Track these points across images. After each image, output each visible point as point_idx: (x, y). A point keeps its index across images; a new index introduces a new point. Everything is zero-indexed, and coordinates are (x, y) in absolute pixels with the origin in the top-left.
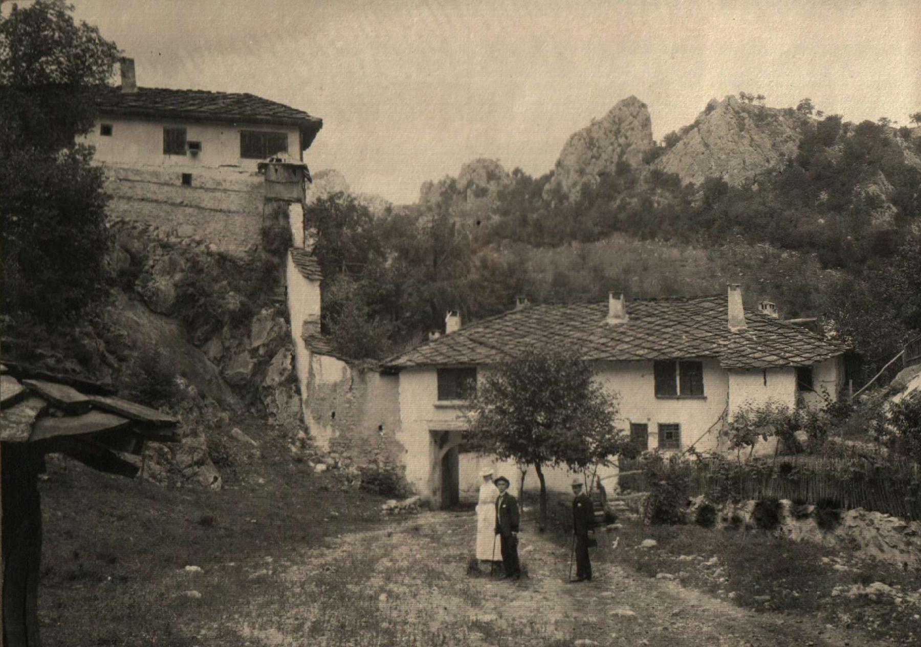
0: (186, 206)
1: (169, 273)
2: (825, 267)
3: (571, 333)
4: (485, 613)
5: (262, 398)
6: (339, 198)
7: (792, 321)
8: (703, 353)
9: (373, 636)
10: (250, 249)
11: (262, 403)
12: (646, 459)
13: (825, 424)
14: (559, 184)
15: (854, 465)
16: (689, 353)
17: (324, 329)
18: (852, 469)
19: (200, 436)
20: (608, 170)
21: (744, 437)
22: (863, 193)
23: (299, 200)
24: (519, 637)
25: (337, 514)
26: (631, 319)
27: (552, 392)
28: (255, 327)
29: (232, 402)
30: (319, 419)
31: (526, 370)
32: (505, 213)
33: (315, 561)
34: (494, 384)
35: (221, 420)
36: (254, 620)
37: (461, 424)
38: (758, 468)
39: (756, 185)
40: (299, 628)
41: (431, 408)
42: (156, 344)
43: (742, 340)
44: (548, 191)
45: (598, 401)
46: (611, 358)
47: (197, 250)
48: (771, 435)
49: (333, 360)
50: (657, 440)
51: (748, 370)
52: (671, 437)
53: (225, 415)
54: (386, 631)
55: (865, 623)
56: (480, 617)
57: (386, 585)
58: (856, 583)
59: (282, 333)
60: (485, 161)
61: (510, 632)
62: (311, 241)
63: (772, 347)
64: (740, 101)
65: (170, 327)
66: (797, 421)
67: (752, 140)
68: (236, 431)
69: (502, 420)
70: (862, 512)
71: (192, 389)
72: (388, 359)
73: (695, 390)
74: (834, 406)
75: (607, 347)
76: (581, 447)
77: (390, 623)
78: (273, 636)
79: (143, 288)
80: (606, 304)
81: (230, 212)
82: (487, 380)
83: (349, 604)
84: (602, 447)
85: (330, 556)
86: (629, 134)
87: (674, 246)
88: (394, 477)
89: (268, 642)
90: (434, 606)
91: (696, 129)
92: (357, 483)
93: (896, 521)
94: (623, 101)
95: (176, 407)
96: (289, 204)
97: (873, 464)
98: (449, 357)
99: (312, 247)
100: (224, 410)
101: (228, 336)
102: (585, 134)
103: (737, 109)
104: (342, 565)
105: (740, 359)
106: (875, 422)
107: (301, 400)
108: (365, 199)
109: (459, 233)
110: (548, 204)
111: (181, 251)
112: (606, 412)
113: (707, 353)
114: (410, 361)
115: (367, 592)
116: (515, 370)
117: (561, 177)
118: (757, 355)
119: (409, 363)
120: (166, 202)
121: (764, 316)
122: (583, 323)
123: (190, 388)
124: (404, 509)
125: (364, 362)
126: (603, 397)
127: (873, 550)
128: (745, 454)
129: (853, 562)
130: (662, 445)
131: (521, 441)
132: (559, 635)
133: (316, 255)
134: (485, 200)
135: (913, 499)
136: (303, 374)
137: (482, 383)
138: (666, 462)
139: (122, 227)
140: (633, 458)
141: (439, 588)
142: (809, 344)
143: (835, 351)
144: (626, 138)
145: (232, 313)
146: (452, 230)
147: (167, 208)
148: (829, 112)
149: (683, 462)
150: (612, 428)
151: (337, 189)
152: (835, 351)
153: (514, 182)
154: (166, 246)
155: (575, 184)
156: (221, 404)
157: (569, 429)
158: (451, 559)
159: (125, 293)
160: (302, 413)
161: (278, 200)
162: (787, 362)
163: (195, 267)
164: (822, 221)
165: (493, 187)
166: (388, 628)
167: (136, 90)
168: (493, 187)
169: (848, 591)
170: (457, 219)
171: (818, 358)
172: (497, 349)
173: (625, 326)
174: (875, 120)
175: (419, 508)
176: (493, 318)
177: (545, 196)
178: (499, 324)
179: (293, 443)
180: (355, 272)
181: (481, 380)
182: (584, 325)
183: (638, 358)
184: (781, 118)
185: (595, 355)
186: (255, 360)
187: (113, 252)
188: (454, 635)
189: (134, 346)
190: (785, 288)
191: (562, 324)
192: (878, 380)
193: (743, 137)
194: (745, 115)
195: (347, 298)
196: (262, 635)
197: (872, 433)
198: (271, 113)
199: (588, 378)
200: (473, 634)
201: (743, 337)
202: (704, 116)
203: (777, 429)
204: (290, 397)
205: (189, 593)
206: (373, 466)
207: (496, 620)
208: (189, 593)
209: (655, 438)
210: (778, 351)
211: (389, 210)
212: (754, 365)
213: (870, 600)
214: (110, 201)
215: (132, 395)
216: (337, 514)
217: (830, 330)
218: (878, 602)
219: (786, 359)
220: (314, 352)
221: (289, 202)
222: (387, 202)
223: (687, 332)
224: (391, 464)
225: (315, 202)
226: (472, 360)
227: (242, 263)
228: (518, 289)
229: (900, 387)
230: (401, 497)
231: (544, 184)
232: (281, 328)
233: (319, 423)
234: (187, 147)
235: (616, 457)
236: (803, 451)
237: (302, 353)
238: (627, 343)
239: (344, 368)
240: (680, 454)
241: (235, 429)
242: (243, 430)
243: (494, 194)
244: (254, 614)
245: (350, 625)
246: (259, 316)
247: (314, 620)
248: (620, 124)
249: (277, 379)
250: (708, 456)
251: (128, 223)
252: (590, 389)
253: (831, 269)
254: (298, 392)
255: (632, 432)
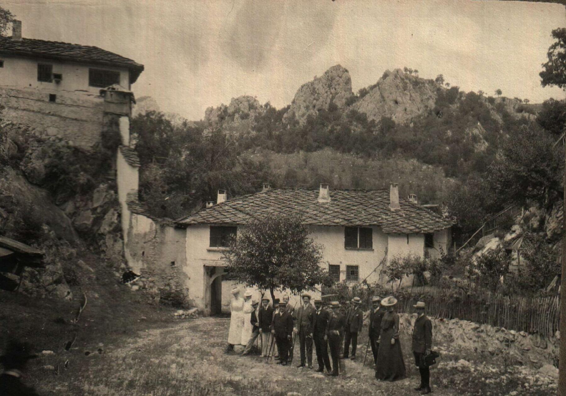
0: (53, 115)
1: (41, 159)
2: (447, 176)
3: (296, 206)
4: (236, 375)
5: (98, 241)
6: (153, 115)
7: (425, 206)
8: (373, 223)
9: (164, 390)
10: (94, 145)
11: (97, 243)
12: (338, 287)
13: (441, 268)
14: (294, 114)
15: (456, 293)
16: (365, 223)
17: (140, 198)
18: (455, 296)
19: (57, 265)
20: (324, 108)
21: (396, 274)
22: (470, 133)
23: (127, 115)
24: (254, 390)
25: (145, 318)
26: (332, 200)
27: (283, 244)
28: (96, 195)
29: (78, 242)
30: (134, 255)
31: (267, 229)
32: (259, 130)
33: (131, 346)
34: (248, 238)
35: (72, 254)
36: (91, 380)
37: (224, 262)
38: (403, 294)
39: (412, 123)
40: (120, 384)
41: (205, 251)
42: (32, 203)
43: (397, 216)
44: (286, 118)
45: (311, 250)
46: (319, 224)
47: (60, 144)
48: (411, 273)
49: (145, 218)
50: (345, 275)
51: (399, 234)
52: (354, 274)
53: (74, 251)
54: (174, 386)
55: (455, 384)
56: (232, 378)
57: (176, 359)
58: (451, 360)
59: (112, 200)
60: (248, 97)
61: (249, 387)
62: (134, 142)
63: (413, 221)
64: (404, 72)
65: (42, 193)
66: (425, 265)
67: (411, 96)
68: (81, 262)
69: (251, 260)
70: (457, 321)
71: (53, 233)
72: (180, 219)
73: (367, 245)
74: (445, 257)
75: (317, 216)
76: (299, 278)
77: (177, 381)
78: (102, 389)
79: (25, 167)
80: (318, 191)
81: (82, 120)
82: (243, 235)
83: (152, 370)
84: (312, 279)
85: (141, 342)
86: (337, 87)
87: (362, 157)
88: (182, 296)
89: (99, 393)
90: (204, 371)
91: (377, 87)
92: (158, 299)
93: (474, 325)
94: (333, 67)
95: (42, 245)
96: (120, 117)
97: (466, 293)
98: (218, 219)
99: (135, 146)
100: (74, 248)
101: (79, 200)
102: (310, 85)
103: (403, 77)
104: (148, 348)
105: (395, 227)
106: (468, 267)
107: (123, 243)
108: (169, 116)
109: (228, 141)
110: (285, 126)
111: (49, 145)
112: (315, 257)
113: (375, 223)
114: (194, 220)
115: (163, 363)
116: (260, 229)
117: (295, 110)
118: (405, 226)
119: (193, 222)
120: (39, 112)
121: (409, 202)
122: (303, 201)
123: (51, 233)
124: (188, 315)
125: (164, 220)
126: (313, 248)
127: (460, 342)
128: (397, 285)
129: (450, 349)
130: (348, 278)
131: (262, 274)
132: (279, 389)
133: (138, 151)
134: (245, 121)
135: (485, 313)
136: (125, 226)
137: (240, 237)
138: (350, 289)
139: (12, 127)
140: (330, 286)
141: (208, 360)
142: (432, 220)
143: (446, 225)
144: (335, 89)
145: (82, 185)
146: (224, 139)
147: (40, 115)
148: (453, 84)
149: (360, 290)
150: (318, 267)
151: (151, 109)
152: (446, 225)
153: (265, 111)
154: (39, 141)
155: (303, 115)
156: (72, 244)
157: (293, 267)
158: (215, 345)
159: (14, 170)
160: (124, 252)
161: (112, 114)
162: (420, 230)
163: (58, 154)
164: (448, 148)
165: (252, 114)
166: (175, 384)
167: (21, 40)
168: (252, 114)
169: (447, 365)
170: (227, 132)
171: (438, 229)
172: (250, 215)
173: (329, 204)
174: (476, 91)
175: (197, 315)
176: (249, 195)
177: (284, 121)
178: (252, 199)
179: (118, 271)
180: (161, 163)
181: (239, 234)
182: (304, 202)
183: (335, 224)
184: (426, 85)
185: (310, 221)
186: (94, 216)
187: (6, 143)
188: (214, 389)
189: (18, 203)
190: (423, 187)
191: (291, 201)
192: (469, 243)
193: (406, 94)
194: (407, 81)
195: (155, 180)
196: (95, 389)
197: (467, 274)
198: (109, 59)
199: (305, 236)
200: (228, 388)
201: (397, 214)
202: (382, 80)
203: (414, 270)
204: (115, 241)
205: (45, 367)
206: (168, 288)
207: (242, 380)
208: (45, 367)
209: (344, 274)
210: (416, 224)
211: (185, 124)
212: (403, 232)
213: (458, 370)
214: (3, 110)
215: (14, 235)
216: (145, 318)
217: (445, 212)
218: (462, 372)
219: (420, 228)
220: (133, 212)
221: (120, 115)
222: (184, 119)
223: (365, 210)
224: (180, 287)
225: (137, 116)
226: (234, 222)
227: (89, 154)
228: (265, 179)
229: (481, 247)
230: (187, 308)
231: (283, 114)
232: (112, 196)
233: (134, 258)
234: (52, 77)
235: (320, 286)
236: (427, 284)
237: (126, 213)
238: (329, 214)
239: (151, 223)
240: (358, 285)
241: (81, 261)
242: (85, 261)
243: (253, 118)
244: (91, 376)
245: (151, 382)
246: (98, 189)
247: (130, 379)
248: (332, 81)
249: (107, 229)
250: (374, 286)
251: (15, 125)
252: (306, 242)
253: (450, 177)
254: (122, 238)
255: (330, 270)
